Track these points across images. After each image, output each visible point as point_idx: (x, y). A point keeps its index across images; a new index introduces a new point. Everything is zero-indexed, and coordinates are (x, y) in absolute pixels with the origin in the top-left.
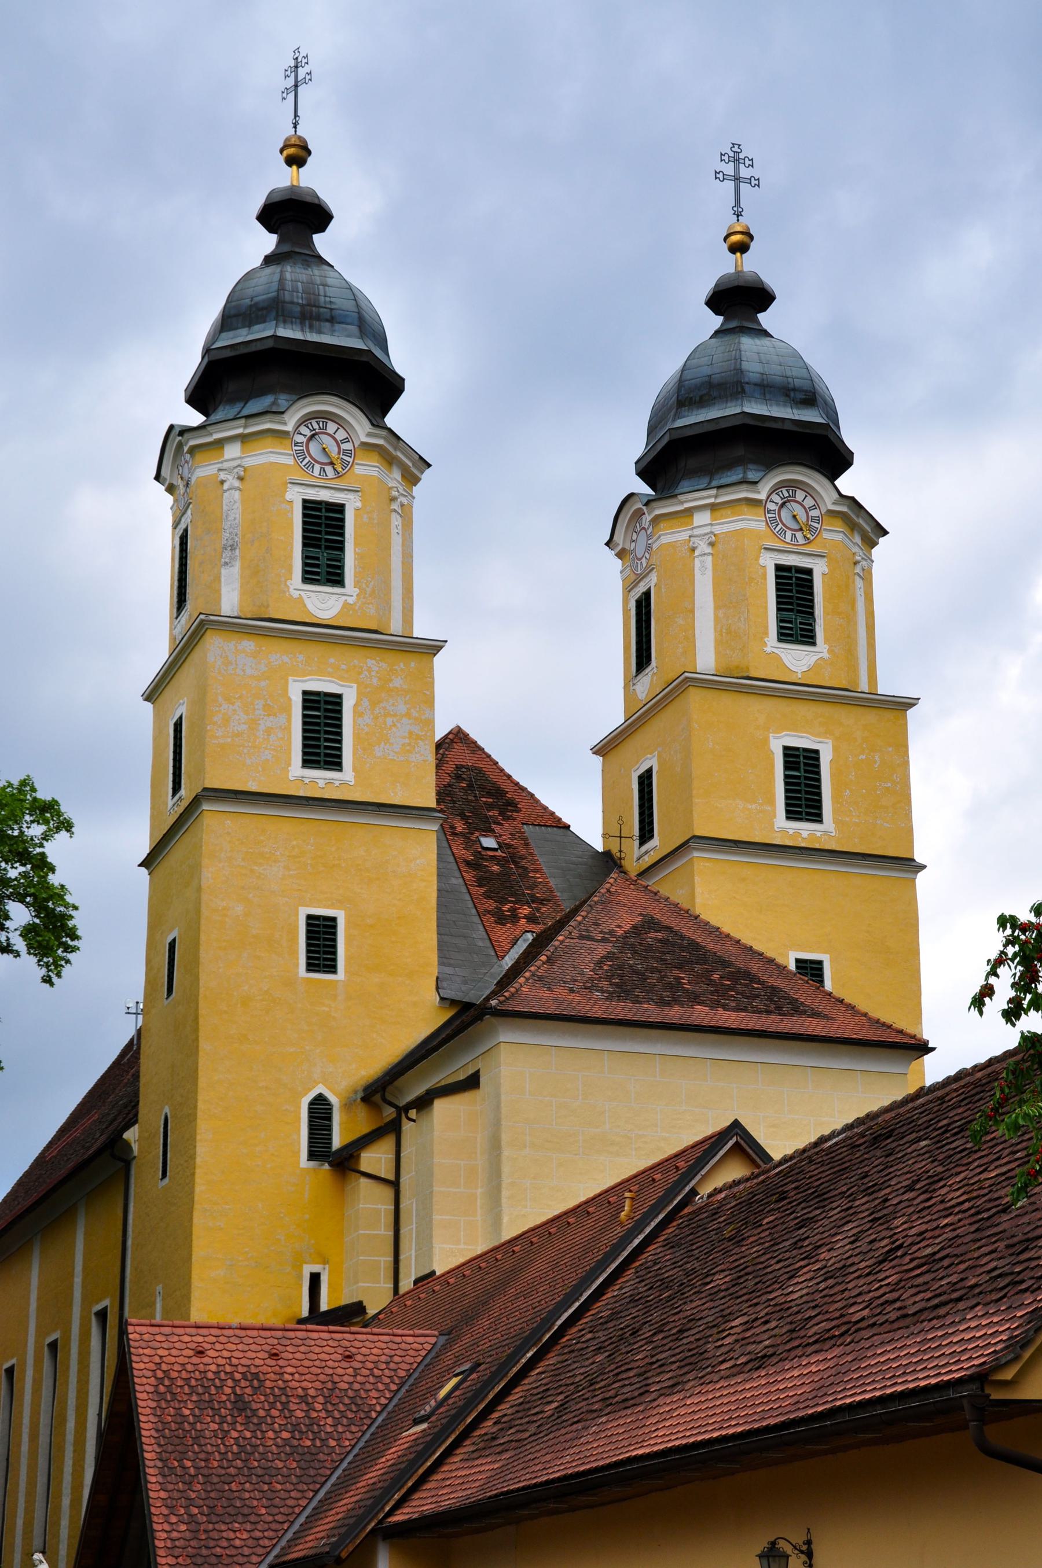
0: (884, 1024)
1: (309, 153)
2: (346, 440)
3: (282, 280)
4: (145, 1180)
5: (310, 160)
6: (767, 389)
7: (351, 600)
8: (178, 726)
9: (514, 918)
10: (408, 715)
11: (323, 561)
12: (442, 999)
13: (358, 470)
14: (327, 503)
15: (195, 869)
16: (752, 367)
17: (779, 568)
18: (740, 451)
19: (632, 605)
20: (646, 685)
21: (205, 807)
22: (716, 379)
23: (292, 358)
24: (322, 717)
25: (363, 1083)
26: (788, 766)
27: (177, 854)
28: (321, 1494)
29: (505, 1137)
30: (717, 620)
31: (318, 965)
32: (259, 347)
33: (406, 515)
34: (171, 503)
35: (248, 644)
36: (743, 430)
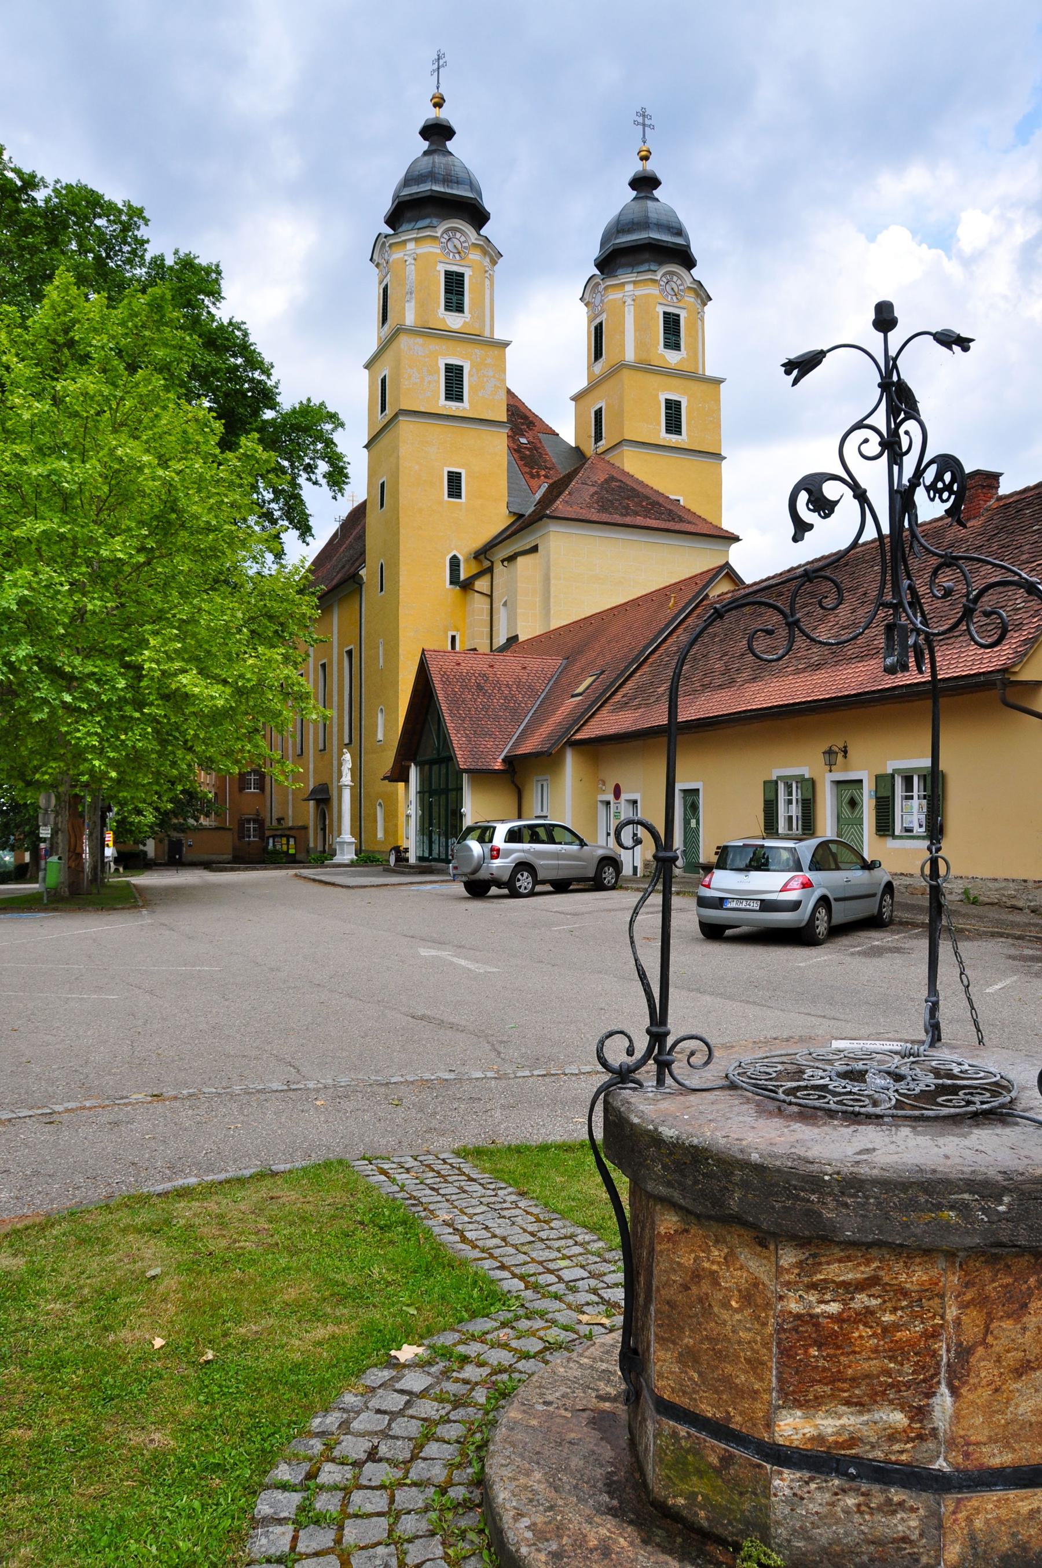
2: (465, 242)
3: (434, 162)
4: (370, 592)
6: (660, 226)
8: (383, 381)
9: (539, 476)
10: (494, 377)
11: (454, 301)
13: (471, 256)
15: (395, 448)
16: (653, 216)
17: (665, 313)
18: (647, 256)
19: (593, 329)
20: (599, 368)
21: (401, 418)
22: (636, 220)
23: (436, 201)
24: (454, 377)
25: (474, 550)
27: (384, 441)
28: (522, 727)
29: (552, 575)
32: (424, 195)
33: (491, 279)
35: (420, 340)
36: (644, 247)
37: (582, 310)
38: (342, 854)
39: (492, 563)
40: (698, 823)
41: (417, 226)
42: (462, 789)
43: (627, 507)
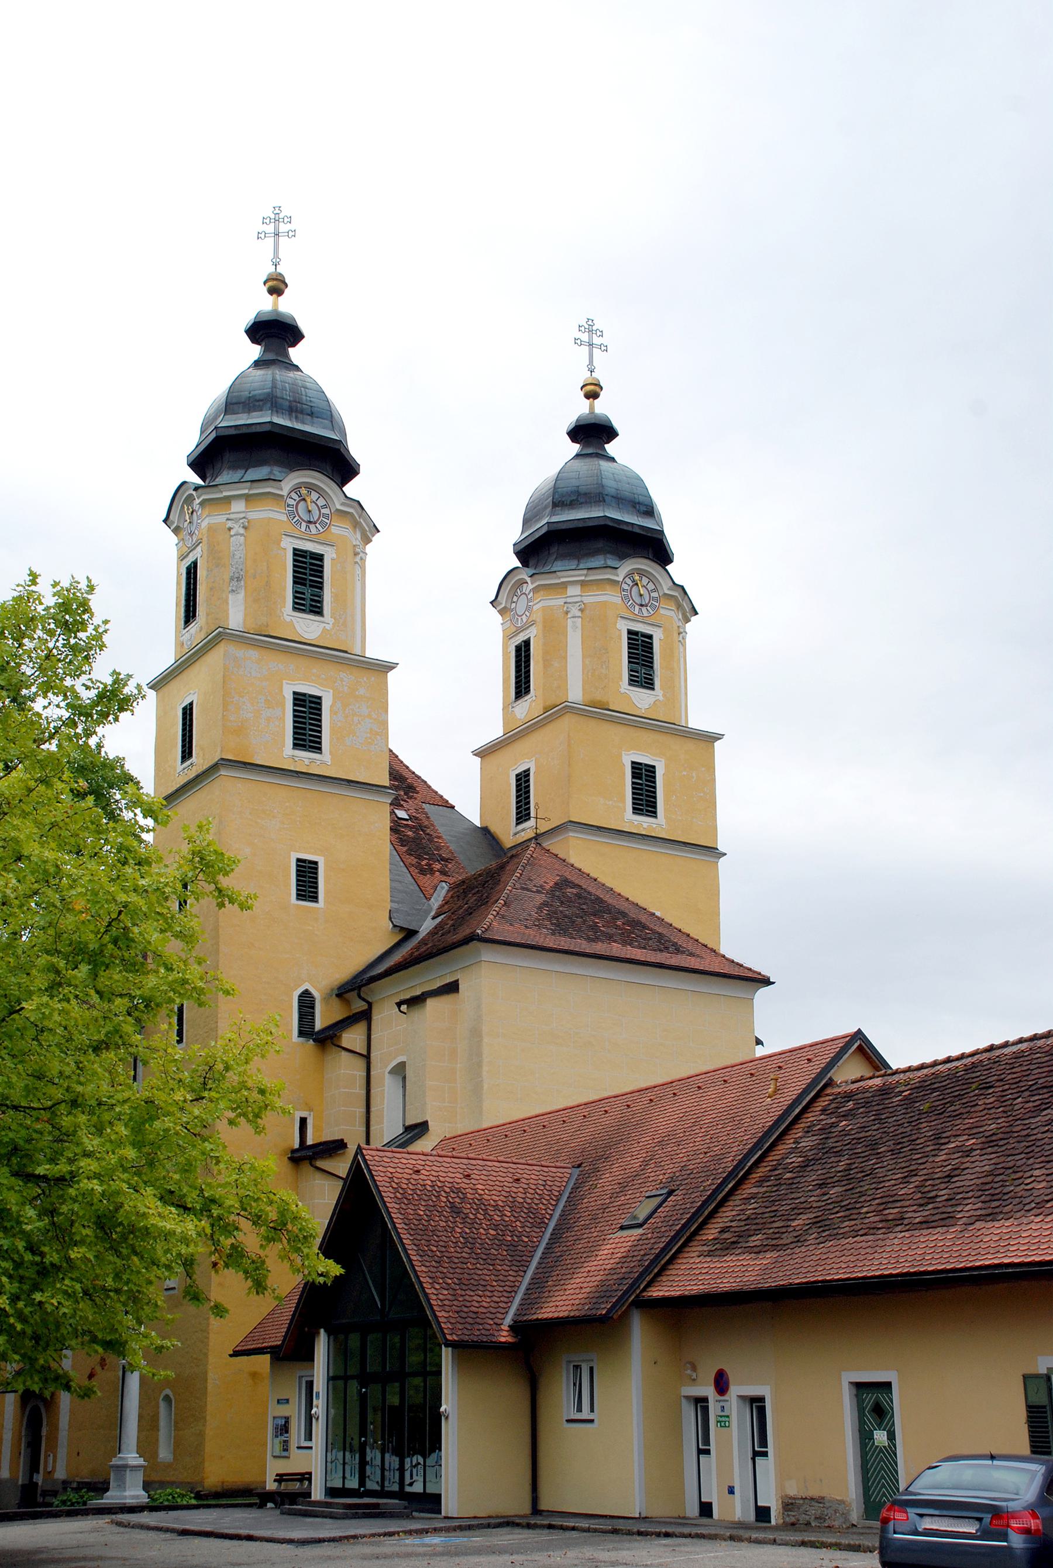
0: (738, 964)
1: (286, 286)
3: (274, 380)
5: (286, 291)
7: (328, 627)
9: (432, 872)
11: (308, 596)
12: (395, 926)
14: (312, 553)
16: (610, 485)
18: (600, 544)
20: (525, 709)
22: (583, 489)
24: (307, 713)
26: (635, 775)
31: (304, 896)
32: (259, 429)
34: (176, 541)
35: (253, 654)
37: (494, 619)
38: (122, 1486)
39: (370, 1004)
40: (891, 1436)
41: (248, 477)
42: (439, 1373)
43: (594, 928)
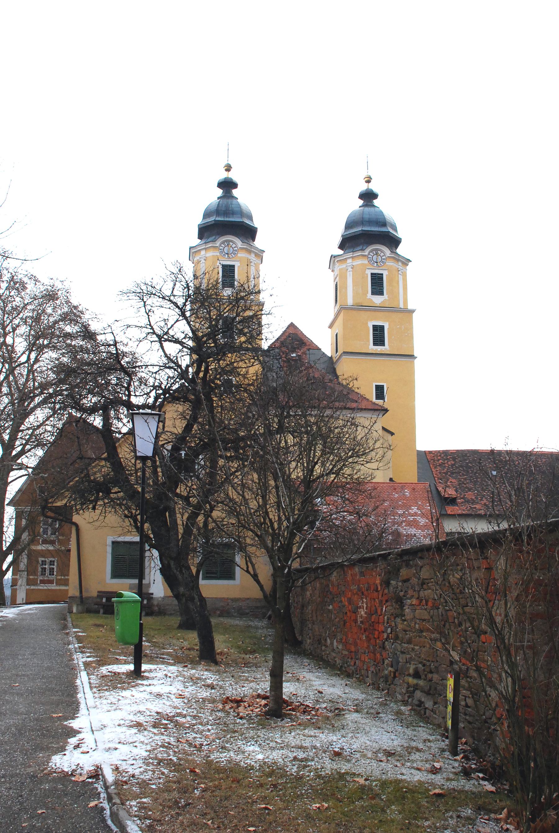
5: (372, 181)
13: (239, 255)
17: (372, 274)
26: (374, 330)
30: (353, 290)
